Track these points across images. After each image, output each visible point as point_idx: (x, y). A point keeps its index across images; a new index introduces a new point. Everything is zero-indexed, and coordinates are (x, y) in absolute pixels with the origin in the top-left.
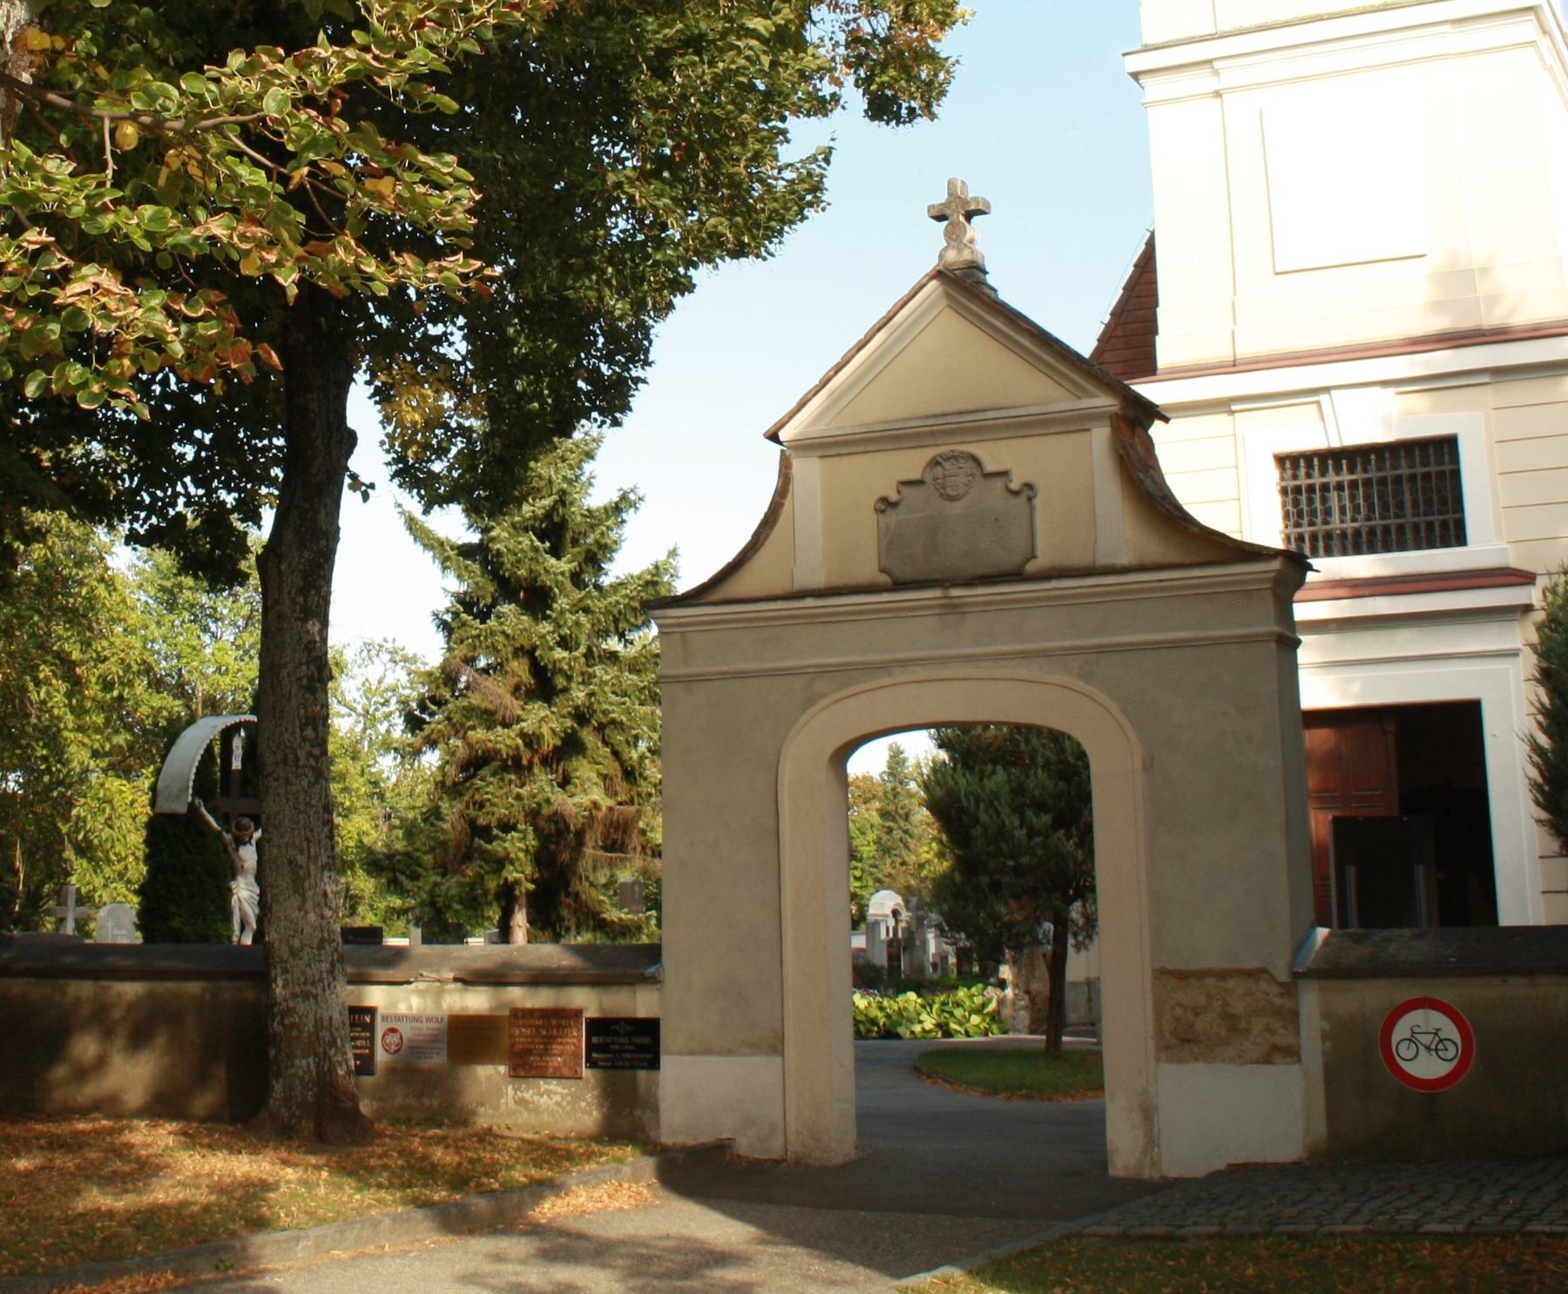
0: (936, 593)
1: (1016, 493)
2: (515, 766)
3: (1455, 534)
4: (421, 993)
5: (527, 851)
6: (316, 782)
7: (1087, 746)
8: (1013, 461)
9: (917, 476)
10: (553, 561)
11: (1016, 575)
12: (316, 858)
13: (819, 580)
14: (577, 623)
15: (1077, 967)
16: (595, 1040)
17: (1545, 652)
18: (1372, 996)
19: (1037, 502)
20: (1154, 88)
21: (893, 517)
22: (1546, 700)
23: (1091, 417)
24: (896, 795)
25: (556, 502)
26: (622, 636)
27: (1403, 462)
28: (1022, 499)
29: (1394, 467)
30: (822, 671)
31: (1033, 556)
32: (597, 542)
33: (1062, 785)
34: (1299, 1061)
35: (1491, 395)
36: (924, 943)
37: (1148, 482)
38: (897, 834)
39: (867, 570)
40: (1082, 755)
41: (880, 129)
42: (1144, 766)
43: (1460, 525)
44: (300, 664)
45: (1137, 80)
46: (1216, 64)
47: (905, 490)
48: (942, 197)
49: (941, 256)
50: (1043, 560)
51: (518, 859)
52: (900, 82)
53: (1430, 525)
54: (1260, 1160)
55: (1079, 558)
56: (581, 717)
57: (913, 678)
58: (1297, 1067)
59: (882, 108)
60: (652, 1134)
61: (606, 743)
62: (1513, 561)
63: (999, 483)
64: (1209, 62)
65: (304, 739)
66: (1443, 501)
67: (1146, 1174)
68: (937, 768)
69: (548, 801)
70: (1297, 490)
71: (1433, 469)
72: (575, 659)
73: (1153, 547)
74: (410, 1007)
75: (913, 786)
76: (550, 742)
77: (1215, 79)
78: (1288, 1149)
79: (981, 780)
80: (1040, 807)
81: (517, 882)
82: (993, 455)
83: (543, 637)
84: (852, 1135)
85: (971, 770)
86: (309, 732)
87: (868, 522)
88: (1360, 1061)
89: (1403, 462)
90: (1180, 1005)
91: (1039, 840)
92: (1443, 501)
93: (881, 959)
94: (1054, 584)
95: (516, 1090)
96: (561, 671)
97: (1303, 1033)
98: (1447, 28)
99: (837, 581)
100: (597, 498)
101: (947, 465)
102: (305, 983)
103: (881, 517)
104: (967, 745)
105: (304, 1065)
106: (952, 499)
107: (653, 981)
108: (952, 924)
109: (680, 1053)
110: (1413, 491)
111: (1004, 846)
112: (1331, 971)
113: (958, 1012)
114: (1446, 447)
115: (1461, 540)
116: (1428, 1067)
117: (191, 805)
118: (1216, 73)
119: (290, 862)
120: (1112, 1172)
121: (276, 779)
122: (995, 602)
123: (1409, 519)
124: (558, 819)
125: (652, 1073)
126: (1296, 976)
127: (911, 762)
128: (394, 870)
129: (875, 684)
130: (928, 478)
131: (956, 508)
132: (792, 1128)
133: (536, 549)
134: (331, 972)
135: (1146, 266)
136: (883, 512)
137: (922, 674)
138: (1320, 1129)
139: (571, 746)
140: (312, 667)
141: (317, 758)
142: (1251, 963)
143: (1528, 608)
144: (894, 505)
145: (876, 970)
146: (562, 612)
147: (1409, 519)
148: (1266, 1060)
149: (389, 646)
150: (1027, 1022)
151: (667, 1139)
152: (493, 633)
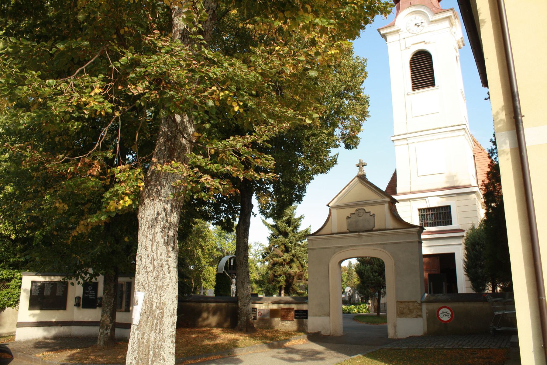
3: (450, 223)
7: (384, 261)
8: (371, 210)
11: (372, 230)
13: (336, 231)
15: (382, 301)
17: (466, 244)
18: (435, 306)
21: (349, 220)
30: (337, 248)
39: (345, 229)
40: (383, 263)
41: (347, 150)
43: (451, 221)
52: (351, 142)
55: (383, 227)
56: (294, 256)
62: (460, 228)
63: (368, 214)
67: (395, 338)
73: (396, 225)
76: (288, 260)
80: (376, 272)
82: (367, 209)
88: (433, 317)
93: (347, 299)
99: (339, 231)
100: (296, 216)
104: (363, 261)
107: (306, 303)
108: (360, 293)
112: (428, 301)
114: (449, 207)
115: (451, 224)
116: (445, 319)
123: (442, 220)
126: (422, 302)
131: (361, 218)
137: (355, 248)
138: (426, 330)
139: (292, 261)
143: (463, 236)
151: (309, 331)
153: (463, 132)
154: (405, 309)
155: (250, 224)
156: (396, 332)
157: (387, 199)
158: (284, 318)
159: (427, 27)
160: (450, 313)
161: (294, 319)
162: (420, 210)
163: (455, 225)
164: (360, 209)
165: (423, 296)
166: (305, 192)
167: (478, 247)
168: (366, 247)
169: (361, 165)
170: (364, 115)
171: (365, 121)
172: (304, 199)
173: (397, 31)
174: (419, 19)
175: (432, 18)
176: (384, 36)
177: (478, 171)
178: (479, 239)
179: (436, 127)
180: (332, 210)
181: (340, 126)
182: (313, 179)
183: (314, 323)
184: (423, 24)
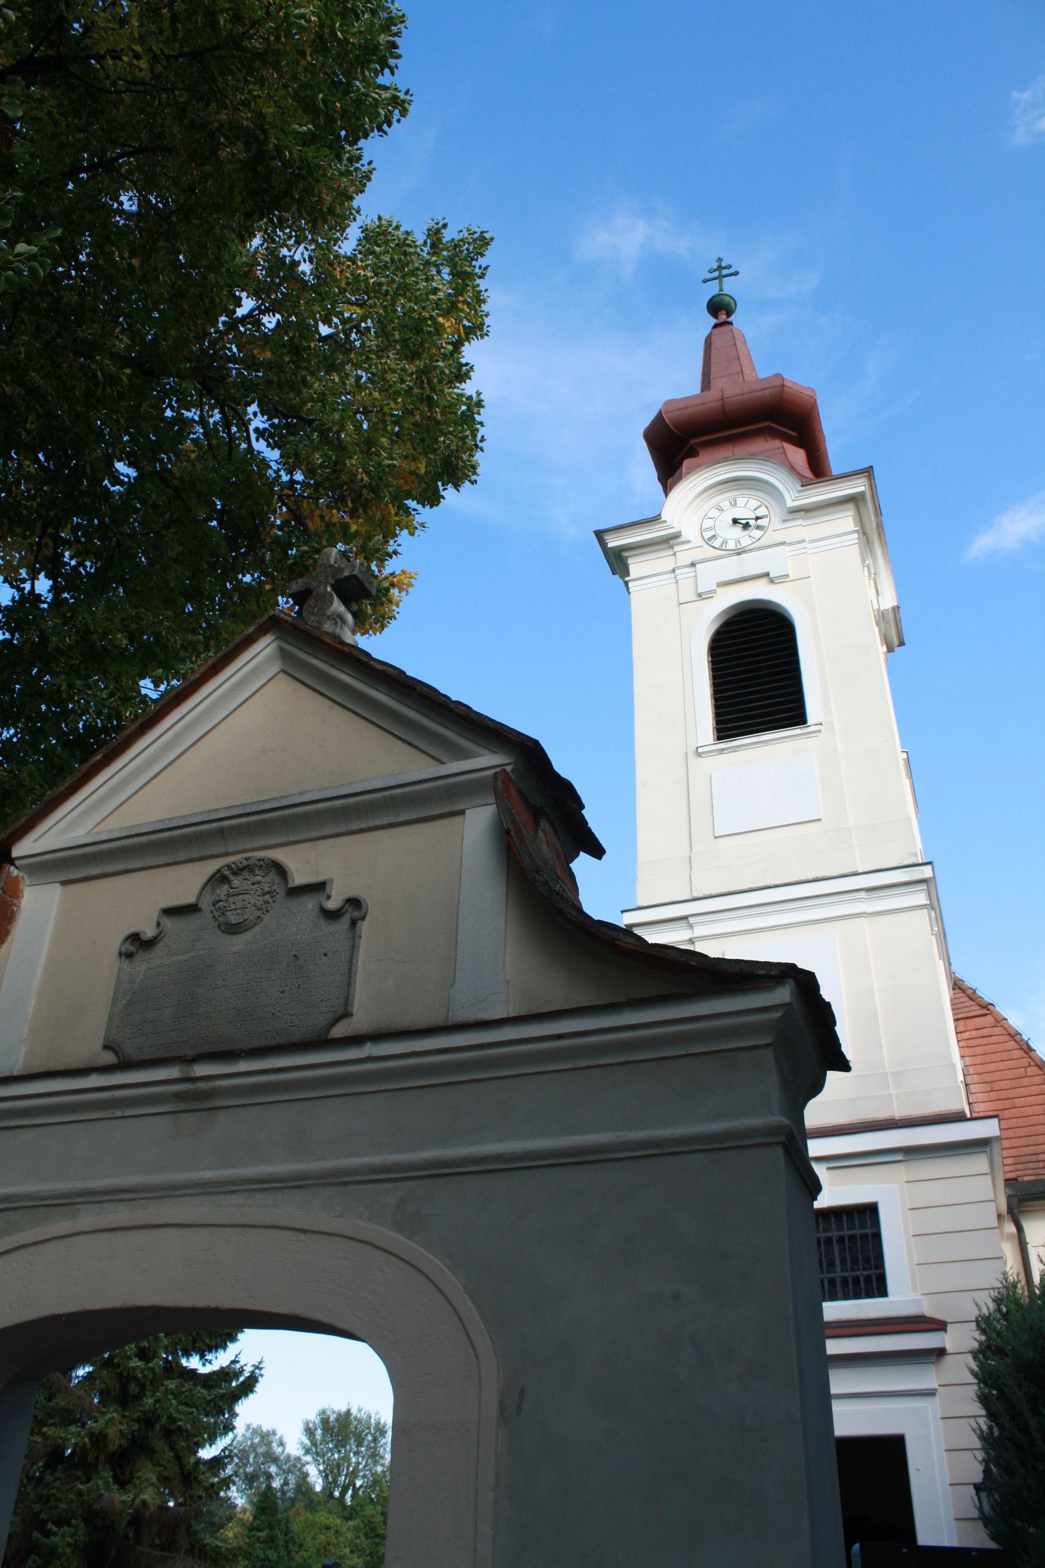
0: (173, 1072)
1: (332, 916)
3: (877, 1287)
9: (191, 899)
17: (986, 1378)
19: (364, 926)
21: (143, 964)
26: (202, 1356)
27: (833, 1226)
29: (826, 1230)
31: (347, 1014)
35: (901, 1172)
42: (502, 1410)
43: (882, 1279)
47: (168, 923)
50: (359, 1021)
51: (65, 1553)
53: (856, 1280)
56: (148, 1421)
61: (172, 1448)
62: (927, 1309)
63: (309, 904)
64: (685, 918)
66: (867, 1260)
73: (556, 988)
76: (115, 1441)
77: (690, 931)
82: (302, 863)
89: (833, 1226)
92: (867, 1260)
96: (136, 1379)
98: (863, 894)
101: (236, 882)
103: (126, 964)
106: (234, 929)
110: (842, 1252)
114: (870, 1211)
115: (883, 1292)
118: (691, 926)
123: (838, 1273)
130: (206, 904)
131: (240, 943)
136: (129, 955)
137: (121, 1214)
143: (941, 1352)
159: (777, 529)
163: (902, 1295)
168: (230, 1208)
173: (669, 541)
174: (747, 505)
175: (793, 495)
176: (618, 562)
179: (811, 877)
184: (759, 522)
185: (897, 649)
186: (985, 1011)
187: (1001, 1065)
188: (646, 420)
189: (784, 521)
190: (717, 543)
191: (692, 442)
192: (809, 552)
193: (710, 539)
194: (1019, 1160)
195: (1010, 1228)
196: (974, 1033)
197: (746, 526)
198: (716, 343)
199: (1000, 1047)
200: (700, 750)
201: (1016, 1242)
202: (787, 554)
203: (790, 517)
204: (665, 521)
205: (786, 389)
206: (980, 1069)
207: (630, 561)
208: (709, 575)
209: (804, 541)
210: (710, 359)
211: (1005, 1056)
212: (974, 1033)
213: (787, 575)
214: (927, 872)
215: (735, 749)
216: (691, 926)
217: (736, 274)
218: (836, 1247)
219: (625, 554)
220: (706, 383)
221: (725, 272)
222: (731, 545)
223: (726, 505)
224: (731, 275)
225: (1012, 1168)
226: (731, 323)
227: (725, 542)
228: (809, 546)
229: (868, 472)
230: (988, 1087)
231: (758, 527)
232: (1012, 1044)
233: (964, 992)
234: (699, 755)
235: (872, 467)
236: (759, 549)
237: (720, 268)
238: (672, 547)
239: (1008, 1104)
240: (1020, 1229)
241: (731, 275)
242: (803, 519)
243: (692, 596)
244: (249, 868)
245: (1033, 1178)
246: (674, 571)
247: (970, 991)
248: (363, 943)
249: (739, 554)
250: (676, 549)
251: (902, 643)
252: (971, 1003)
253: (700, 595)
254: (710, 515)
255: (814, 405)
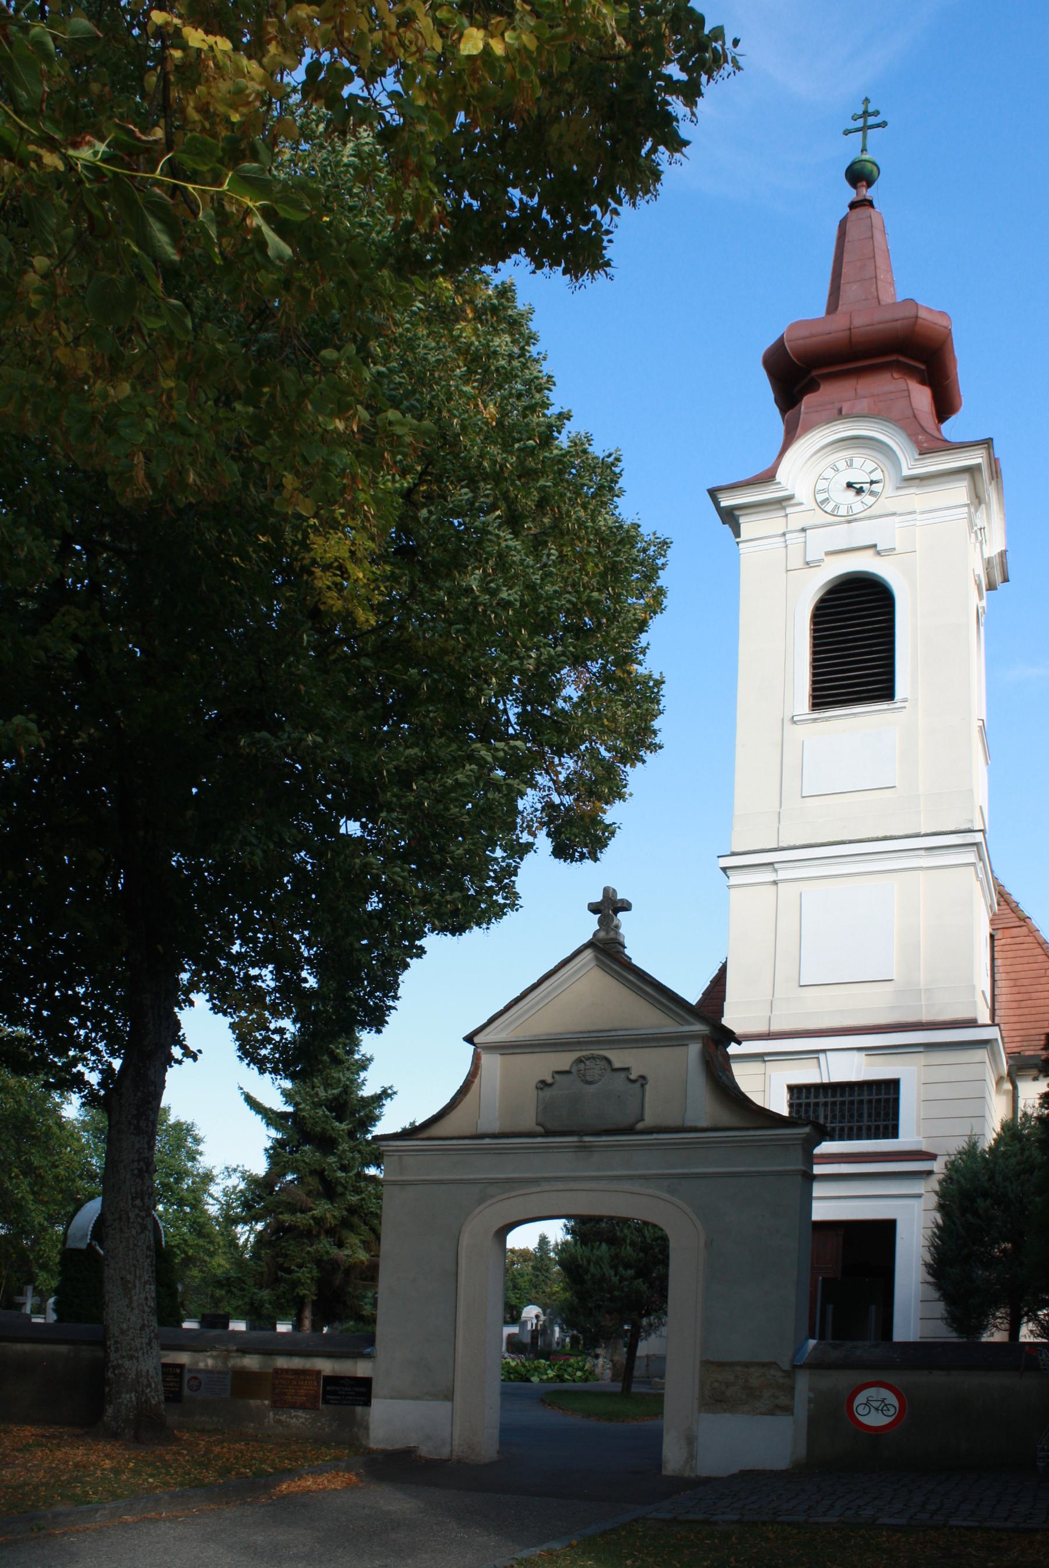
0: (575, 1139)
2: (308, 1235)
3: (893, 1132)
4: (214, 1357)
5: (312, 1279)
6: (142, 1232)
7: (668, 1232)
8: (634, 1060)
9: (567, 1068)
10: (337, 1124)
11: (630, 1130)
12: (140, 1277)
13: (496, 1127)
14: (353, 1158)
15: (644, 1348)
16: (328, 1388)
17: (942, 1195)
18: (844, 1379)
19: (647, 1087)
20: (736, 878)
21: (548, 1093)
22: (940, 1221)
23: (692, 1037)
24: (542, 1260)
25: (341, 1092)
27: (865, 1093)
28: (638, 1085)
30: (493, 1182)
31: (642, 1120)
32: (366, 1115)
33: (641, 1255)
34: (792, 1414)
35: (921, 1059)
36: (553, 1331)
37: (724, 1078)
38: (541, 1278)
39: (528, 1122)
40: (665, 1239)
41: (560, 864)
44: (133, 1161)
45: (725, 873)
46: (776, 866)
47: (557, 1077)
48: (598, 898)
49: (595, 935)
50: (649, 1120)
52: (579, 836)
54: (761, 1467)
55: (672, 1121)
56: (352, 1210)
57: (554, 1188)
58: (791, 1417)
59: (561, 851)
60: (364, 1442)
61: (366, 1224)
62: (924, 1147)
63: (623, 1075)
64: (772, 864)
65: (134, 1206)
67: (686, 1475)
68: (565, 1243)
69: (327, 1252)
70: (800, 1105)
71: (883, 1097)
72: (350, 1177)
73: (725, 1117)
74: (207, 1365)
75: (552, 1255)
77: (774, 874)
78: (781, 1463)
79: (592, 1250)
80: (627, 1267)
81: (304, 1296)
82: (619, 1058)
83: (330, 1164)
84: (496, 1447)
85: (586, 1245)
86: (138, 1202)
87: (532, 1093)
88: (832, 1416)
89: (865, 1093)
90: (716, 1381)
91: (626, 1283)
92: (887, 1114)
93: (527, 1339)
94: (655, 1136)
95: (275, 1415)
97: (796, 1398)
98: (922, 852)
99: (508, 1129)
100: (368, 1091)
101: (588, 1063)
102: (130, 1350)
103: (540, 1092)
104: (585, 1228)
105: (128, 1398)
107: (369, 1356)
108: (568, 1324)
109: (385, 1398)
111: (605, 1285)
112: (818, 1365)
113: (570, 1370)
115: (895, 1135)
116: (875, 1419)
117: (89, 1245)
118: (776, 870)
119: (122, 1279)
120: (664, 1472)
121: (114, 1229)
122: (614, 1146)
123: (865, 1122)
124: (335, 1264)
125: (365, 1408)
126: (795, 1367)
127: (552, 1243)
128: (229, 1286)
129: (528, 1191)
130: (574, 1070)
131: (591, 1089)
132: (456, 1442)
133: (327, 1116)
134: (149, 1344)
135: (723, 970)
137: (560, 1186)
138: (802, 1452)
139: (345, 1224)
140: (142, 1163)
141: (143, 1218)
142: (766, 1360)
143: (930, 1173)
144: (550, 1085)
145: (524, 1345)
146: (344, 1151)
147: (865, 1122)
148: (771, 1413)
149: (240, 1169)
150: (610, 1376)
151: (373, 1445)
152: (297, 1161)
153: (971, 857)
154: (728, 1387)
155: (164, 1088)
156: (692, 1456)
157: (699, 1028)
158: (280, 1403)
159: (890, 498)
160: (896, 1403)
161: (321, 1406)
162: (791, 1088)
163: (908, 1138)
164: (593, 1058)
165: (800, 1347)
166: (396, 998)
167: (981, 1204)
169: (609, 907)
170: (638, 740)
171: (639, 765)
172: (392, 1018)
173: (782, 503)
174: (863, 467)
175: (910, 464)
176: (730, 517)
177: (999, 984)
178: (991, 1178)
179: (881, 835)
180: (488, 1060)
181: (542, 780)
182: (421, 952)
183: (388, 1420)
184: (875, 487)
185: (1001, 586)
186: (1022, 923)
187: (1026, 967)
188: (769, 341)
189: (898, 488)
190: (829, 508)
191: (814, 373)
192: (918, 523)
193: (823, 502)
194: (1026, 1038)
195: (1008, 1086)
196: (1009, 941)
197: (859, 491)
198: (852, 233)
199: (1029, 953)
200: (795, 719)
201: (1011, 1095)
202: (897, 526)
203: (905, 484)
204: (779, 483)
205: (920, 321)
206: (1009, 969)
207: (742, 520)
208: (819, 542)
209: (914, 512)
210: (842, 253)
211: (1031, 960)
212: (1009, 941)
213: (894, 549)
214: (978, 837)
215: (827, 719)
216: (776, 870)
217: (883, 125)
218: (865, 1106)
219: (737, 513)
220: (833, 304)
221: (871, 121)
222: (842, 511)
223: (841, 465)
224: (878, 126)
225: (1018, 1044)
226: (869, 203)
227: (837, 507)
228: (919, 517)
229: (987, 443)
230: (1012, 983)
231: (872, 493)
232: (1039, 951)
233: (1008, 905)
234: (795, 722)
235: (992, 439)
236: (870, 518)
237: (866, 114)
238: (784, 508)
239: (1026, 996)
240: (1015, 1087)
241: (878, 126)
242: (918, 487)
243: (800, 564)
244: (593, 1058)
245: (1032, 1053)
246: (784, 534)
247: (1014, 905)
248: (647, 1094)
249: (849, 522)
250: (789, 510)
251: (1006, 580)
252: (1013, 915)
253: (807, 563)
254: (825, 475)
255: (949, 333)
